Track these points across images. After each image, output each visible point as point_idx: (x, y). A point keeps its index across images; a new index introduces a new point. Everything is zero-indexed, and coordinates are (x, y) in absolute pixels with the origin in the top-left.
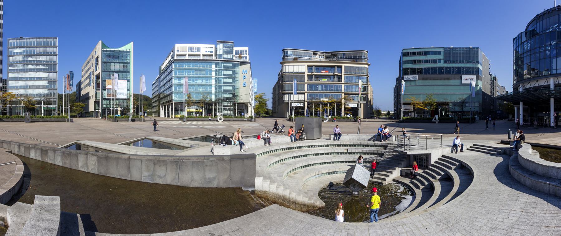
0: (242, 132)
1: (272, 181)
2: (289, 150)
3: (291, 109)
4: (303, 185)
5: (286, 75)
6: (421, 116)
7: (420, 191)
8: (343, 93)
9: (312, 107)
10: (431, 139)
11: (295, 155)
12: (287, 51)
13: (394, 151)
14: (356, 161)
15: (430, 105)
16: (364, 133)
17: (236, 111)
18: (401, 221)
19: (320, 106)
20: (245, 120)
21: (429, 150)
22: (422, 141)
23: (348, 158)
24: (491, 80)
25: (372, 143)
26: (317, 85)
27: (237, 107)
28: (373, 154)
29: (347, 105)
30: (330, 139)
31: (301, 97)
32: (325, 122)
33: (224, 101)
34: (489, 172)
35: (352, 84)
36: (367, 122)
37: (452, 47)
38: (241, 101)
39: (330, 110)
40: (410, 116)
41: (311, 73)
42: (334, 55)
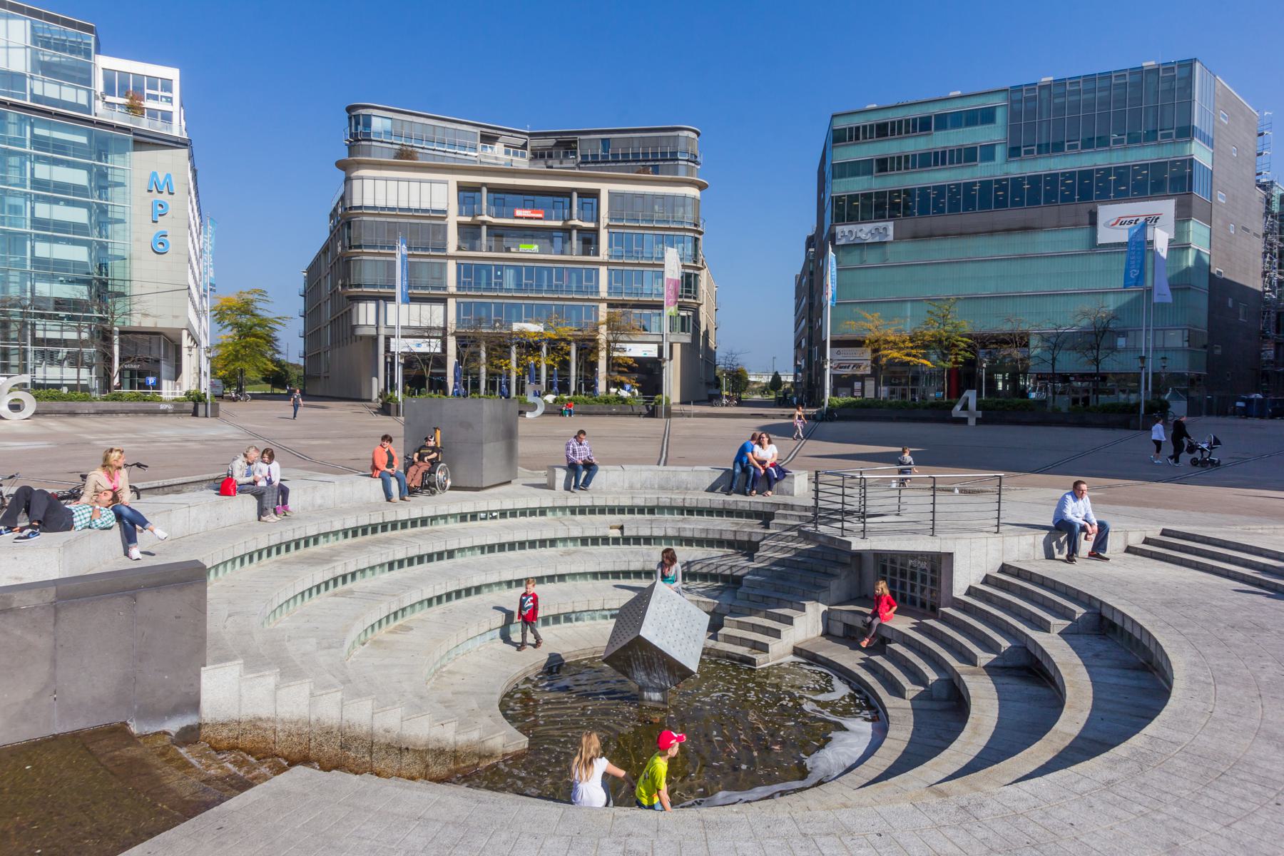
0: (139, 465)
1: (289, 671)
2: (376, 536)
3: (390, 366)
4: (436, 672)
5: (365, 218)
6: (904, 396)
7: (908, 704)
8: (602, 300)
9: (479, 355)
10: (952, 491)
11: (400, 555)
12: (369, 117)
13: (799, 536)
14: (655, 572)
15: (944, 346)
16: (682, 461)
17: (111, 370)
18: (831, 817)
19: (509, 353)
20: (165, 412)
21: (942, 536)
22: (913, 500)
23: (624, 559)
24: (1268, 212)
25: (719, 499)
26: (498, 268)
27: (116, 349)
28: (720, 543)
29: (617, 350)
30: (550, 486)
31: (431, 315)
32: (530, 419)
33: (42, 316)
34: (1264, 678)
35: (639, 265)
36: (692, 419)
37: (1051, 79)
38: (136, 322)
39: (550, 368)
40: (860, 394)
41: (474, 216)
42: (566, 145)
